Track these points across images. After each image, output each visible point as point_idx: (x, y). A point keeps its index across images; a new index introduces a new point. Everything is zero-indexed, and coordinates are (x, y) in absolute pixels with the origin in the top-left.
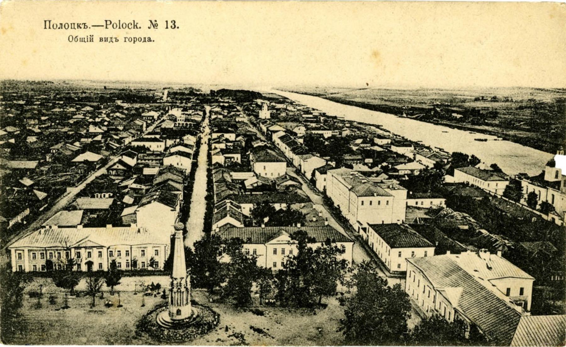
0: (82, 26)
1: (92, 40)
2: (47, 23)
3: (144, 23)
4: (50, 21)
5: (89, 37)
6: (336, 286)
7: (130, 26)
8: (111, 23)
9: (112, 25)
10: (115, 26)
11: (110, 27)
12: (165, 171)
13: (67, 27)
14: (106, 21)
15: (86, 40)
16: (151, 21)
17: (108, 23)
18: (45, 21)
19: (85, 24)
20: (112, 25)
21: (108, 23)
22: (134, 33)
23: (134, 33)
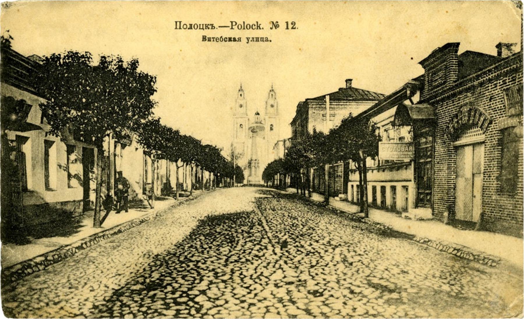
0: (210, 27)
3: (266, 25)
4: (180, 22)
7: (254, 27)
8: (236, 24)
10: (240, 27)
11: (235, 27)
16: (273, 23)
18: (176, 22)
19: (212, 25)
21: (234, 24)
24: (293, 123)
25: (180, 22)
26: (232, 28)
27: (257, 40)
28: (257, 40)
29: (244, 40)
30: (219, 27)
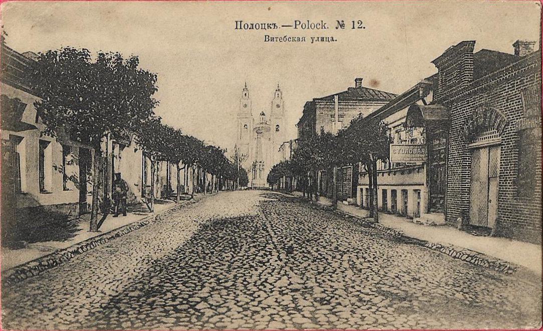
0: (273, 27)
2: (267, 37)
7: (318, 27)
9: (301, 25)
18: (237, 22)
19: (275, 24)
21: (298, 23)
26: (296, 28)
30: (282, 26)
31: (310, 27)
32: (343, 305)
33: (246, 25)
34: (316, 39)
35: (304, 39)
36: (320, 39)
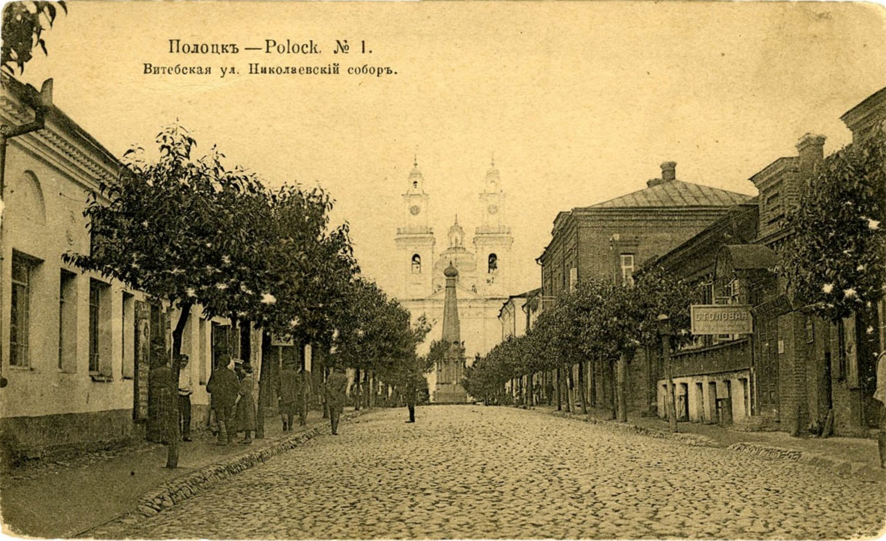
0: (230, 49)
1: (336, 71)
3: (327, 45)
4: (178, 41)
5: (332, 66)
6: (421, 340)
7: (305, 49)
10: (281, 49)
11: (273, 49)
12: (753, 535)
13: (205, 50)
14: (268, 41)
15: (327, 70)
16: (338, 42)
17: (271, 43)
18: (171, 41)
19: (234, 45)
20: (277, 45)
21: (271, 43)
22: (311, 60)
23: (311, 60)
24: (544, 259)
25: (178, 41)
26: (268, 52)
27: (309, 70)
28: (309, 70)
29: (216, 72)
30: (363, 42)
31: (291, 50)
32: (41, 37)
33: (186, 47)
34: (229, 70)
35: (209, 70)
36: (290, 70)
